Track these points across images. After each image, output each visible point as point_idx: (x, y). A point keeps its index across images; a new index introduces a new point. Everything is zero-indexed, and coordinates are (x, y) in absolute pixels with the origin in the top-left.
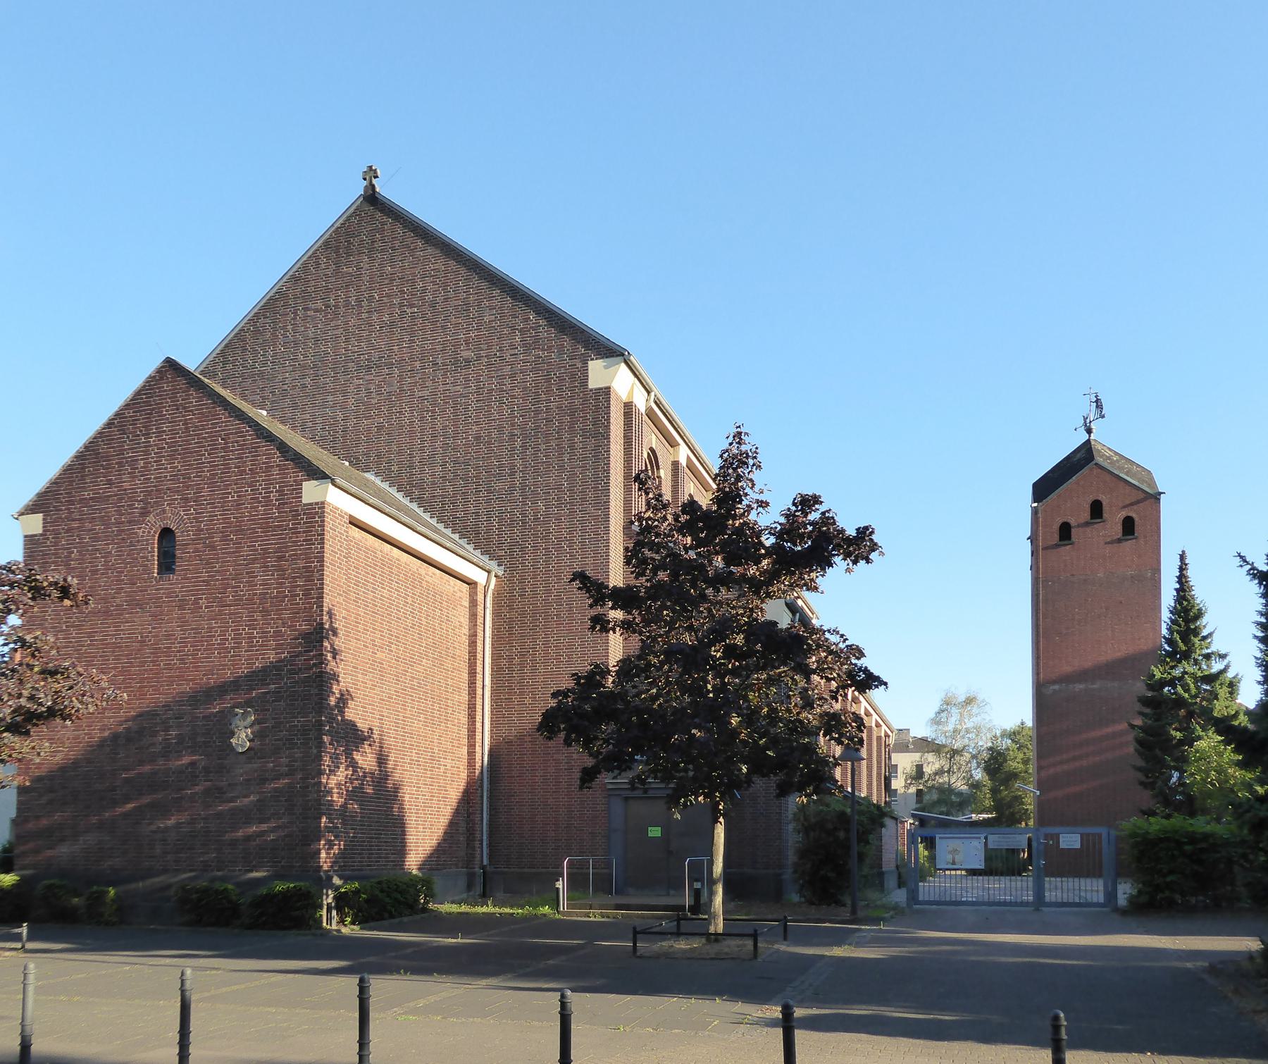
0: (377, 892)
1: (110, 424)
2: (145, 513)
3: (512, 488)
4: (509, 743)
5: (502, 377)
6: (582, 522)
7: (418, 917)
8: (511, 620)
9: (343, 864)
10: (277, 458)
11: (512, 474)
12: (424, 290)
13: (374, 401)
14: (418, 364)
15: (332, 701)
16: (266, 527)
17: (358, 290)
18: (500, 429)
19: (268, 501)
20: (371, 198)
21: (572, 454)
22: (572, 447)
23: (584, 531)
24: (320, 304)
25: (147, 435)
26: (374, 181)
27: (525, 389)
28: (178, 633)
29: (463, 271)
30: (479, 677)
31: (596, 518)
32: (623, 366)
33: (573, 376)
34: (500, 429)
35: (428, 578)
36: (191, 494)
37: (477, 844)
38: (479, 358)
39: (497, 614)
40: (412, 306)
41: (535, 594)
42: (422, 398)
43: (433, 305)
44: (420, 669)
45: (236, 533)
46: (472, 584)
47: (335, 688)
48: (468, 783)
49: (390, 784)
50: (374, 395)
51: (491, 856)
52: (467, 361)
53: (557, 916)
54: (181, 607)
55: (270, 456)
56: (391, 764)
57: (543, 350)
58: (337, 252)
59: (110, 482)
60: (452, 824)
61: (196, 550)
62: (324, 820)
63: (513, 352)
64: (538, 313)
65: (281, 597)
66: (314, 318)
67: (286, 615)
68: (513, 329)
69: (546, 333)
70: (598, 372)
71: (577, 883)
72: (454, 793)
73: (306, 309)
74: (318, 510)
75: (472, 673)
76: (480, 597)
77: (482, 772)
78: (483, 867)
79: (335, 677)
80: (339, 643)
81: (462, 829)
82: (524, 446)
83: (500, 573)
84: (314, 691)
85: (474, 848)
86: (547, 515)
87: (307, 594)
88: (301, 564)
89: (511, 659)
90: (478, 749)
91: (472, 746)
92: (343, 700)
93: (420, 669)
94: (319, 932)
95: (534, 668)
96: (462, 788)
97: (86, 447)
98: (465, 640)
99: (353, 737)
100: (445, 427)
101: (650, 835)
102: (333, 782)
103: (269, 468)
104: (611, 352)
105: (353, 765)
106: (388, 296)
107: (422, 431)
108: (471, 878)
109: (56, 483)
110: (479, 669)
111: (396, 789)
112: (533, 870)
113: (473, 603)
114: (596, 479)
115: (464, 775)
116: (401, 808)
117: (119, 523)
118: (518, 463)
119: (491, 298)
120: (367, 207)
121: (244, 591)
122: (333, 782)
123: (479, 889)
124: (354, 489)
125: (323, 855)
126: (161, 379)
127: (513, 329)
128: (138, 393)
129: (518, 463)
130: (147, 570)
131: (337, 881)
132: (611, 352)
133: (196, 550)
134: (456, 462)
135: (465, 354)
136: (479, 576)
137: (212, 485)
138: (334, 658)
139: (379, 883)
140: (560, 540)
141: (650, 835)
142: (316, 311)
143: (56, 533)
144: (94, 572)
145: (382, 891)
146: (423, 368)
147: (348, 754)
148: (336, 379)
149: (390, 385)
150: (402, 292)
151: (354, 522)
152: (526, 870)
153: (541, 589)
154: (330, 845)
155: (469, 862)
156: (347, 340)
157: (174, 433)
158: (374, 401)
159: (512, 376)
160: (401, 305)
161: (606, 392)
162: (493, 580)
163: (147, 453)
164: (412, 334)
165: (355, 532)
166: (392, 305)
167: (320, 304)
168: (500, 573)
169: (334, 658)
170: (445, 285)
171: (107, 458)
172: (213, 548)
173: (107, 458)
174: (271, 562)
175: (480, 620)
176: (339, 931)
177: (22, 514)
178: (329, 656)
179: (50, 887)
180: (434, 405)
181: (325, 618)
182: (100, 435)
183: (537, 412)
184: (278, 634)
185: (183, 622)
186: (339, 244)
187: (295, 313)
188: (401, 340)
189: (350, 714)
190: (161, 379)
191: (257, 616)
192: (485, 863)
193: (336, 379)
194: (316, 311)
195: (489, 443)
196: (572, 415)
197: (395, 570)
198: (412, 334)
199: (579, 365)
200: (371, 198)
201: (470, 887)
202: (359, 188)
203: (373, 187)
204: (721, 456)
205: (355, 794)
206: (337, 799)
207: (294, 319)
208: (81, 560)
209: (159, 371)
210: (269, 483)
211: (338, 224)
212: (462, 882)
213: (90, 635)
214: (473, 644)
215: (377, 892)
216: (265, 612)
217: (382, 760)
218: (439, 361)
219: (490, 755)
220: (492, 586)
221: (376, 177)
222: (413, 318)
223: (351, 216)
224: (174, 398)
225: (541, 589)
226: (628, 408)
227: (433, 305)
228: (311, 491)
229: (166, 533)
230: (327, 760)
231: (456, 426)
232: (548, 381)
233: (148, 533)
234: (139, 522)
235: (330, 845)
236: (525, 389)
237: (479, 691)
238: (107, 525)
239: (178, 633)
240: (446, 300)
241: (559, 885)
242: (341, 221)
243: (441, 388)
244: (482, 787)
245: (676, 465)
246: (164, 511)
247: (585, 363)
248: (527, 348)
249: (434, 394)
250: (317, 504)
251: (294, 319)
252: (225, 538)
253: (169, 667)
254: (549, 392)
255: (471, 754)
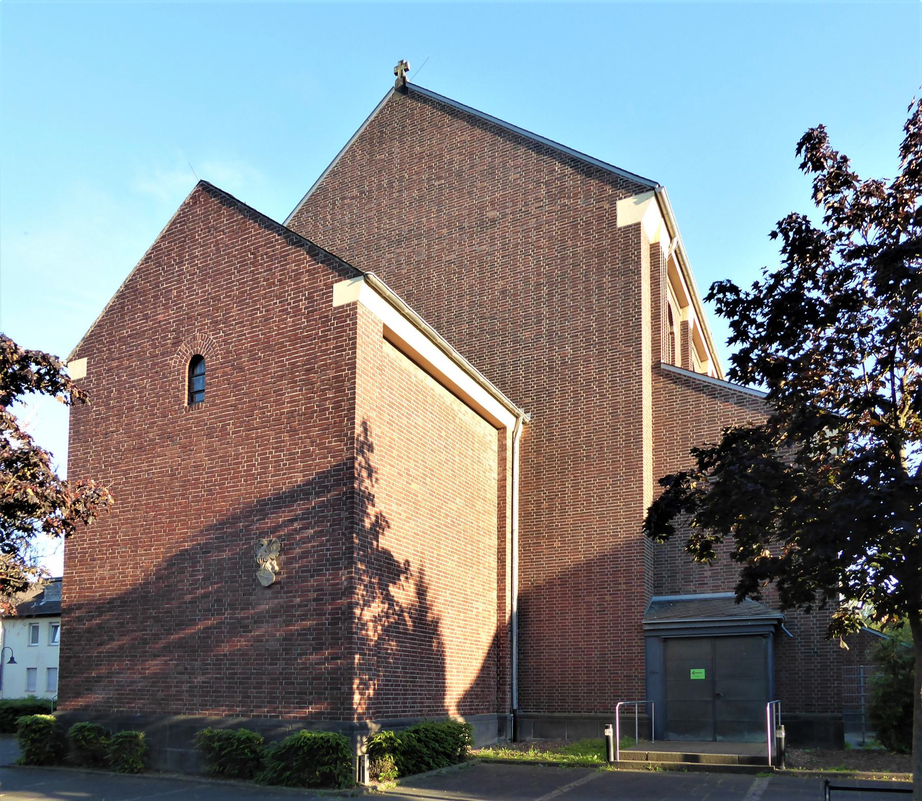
0: (415, 743)
1: (147, 259)
2: (177, 343)
3: (539, 335)
4: (538, 587)
5: (528, 231)
6: (612, 360)
7: (455, 767)
8: (539, 465)
9: (376, 707)
10: (307, 262)
11: (539, 322)
12: (451, 162)
13: (404, 272)
14: (445, 231)
15: (367, 524)
16: (294, 339)
17: (390, 174)
18: (526, 280)
19: (297, 310)
20: (403, 88)
21: (601, 295)
22: (600, 287)
23: (614, 369)
24: (355, 192)
25: (181, 263)
26: (405, 74)
27: (551, 238)
28: (207, 463)
29: (488, 136)
30: (508, 521)
31: (627, 355)
32: (653, 199)
33: (600, 218)
34: (526, 280)
35: (460, 415)
36: (220, 315)
37: (507, 688)
38: (504, 215)
39: (524, 460)
40: (439, 178)
41: (564, 438)
42: (450, 262)
43: (459, 174)
44: (454, 506)
45: (264, 350)
46: (501, 429)
47: (371, 510)
48: (498, 627)
49: (430, 616)
50: (404, 266)
51: (519, 700)
52: (493, 221)
53: (610, 769)
54: (210, 436)
55: (299, 262)
56: (430, 595)
57: (569, 198)
58: (371, 143)
59: (146, 317)
60: (484, 668)
61: (225, 374)
62: (357, 656)
63: (537, 205)
64: (563, 162)
65: (309, 413)
66: (350, 205)
67: (315, 432)
68: (538, 183)
69: (572, 179)
70: (628, 211)
71: (627, 729)
72: (486, 636)
73: (343, 199)
74: (350, 311)
75: (502, 517)
76: (509, 443)
77: (511, 617)
78: (513, 711)
79: (370, 498)
80: (374, 459)
81: (493, 674)
82: (550, 294)
83: (528, 420)
84: (344, 514)
85: (504, 692)
86: (575, 358)
87: (337, 407)
88: (331, 374)
89: (538, 503)
90: (508, 594)
91: (501, 590)
92: (381, 524)
93: (454, 506)
94: (349, 791)
95: (563, 511)
96: (493, 632)
97: (126, 286)
98: (494, 484)
99: (389, 569)
100: (471, 286)
101: (693, 677)
102: (367, 615)
103: (298, 275)
104: (639, 187)
105: (388, 598)
106: (417, 173)
107: (449, 292)
108: (502, 721)
109: (99, 325)
110: (508, 513)
111: (436, 623)
112: (566, 714)
113: (502, 448)
114: (626, 313)
115: (494, 619)
116: (441, 644)
117: (153, 356)
118: (545, 310)
119: (515, 158)
120: (400, 98)
121: (272, 412)
122: (367, 615)
123: (510, 734)
124: (389, 292)
125: (357, 697)
126: (195, 203)
127: (538, 183)
128: (173, 223)
129: (545, 310)
130: (178, 400)
131: (373, 726)
132: (639, 187)
133: (225, 374)
134: (482, 318)
135: (491, 214)
136: (507, 420)
137: (241, 302)
138: (370, 476)
139: (416, 732)
140: (588, 381)
141: (693, 677)
142: (352, 198)
143: (98, 374)
144: (130, 409)
145: (419, 740)
146: (450, 233)
147: (384, 588)
148: (369, 257)
149: (419, 254)
150: (431, 167)
151: (389, 337)
152: (557, 714)
153: (569, 432)
154: (365, 685)
155: (499, 708)
156: (379, 220)
157: (205, 255)
158: (404, 272)
159: (538, 228)
160: (429, 179)
161: (636, 228)
162: (521, 428)
163: (180, 281)
164: (440, 204)
165: (388, 347)
166: (421, 181)
167: (355, 192)
168: (528, 420)
169: (370, 476)
170: (471, 154)
171: (144, 293)
172: (241, 369)
173: (144, 293)
174: (300, 376)
175: (509, 465)
176: (375, 788)
177: (71, 360)
178: (364, 474)
179: (81, 730)
180: (461, 266)
181: (358, 430)
182: (139, 271)
183: (563, 259)
184: (306, 454)
185: (211, 451)
186: (374, 135)
187: (334, 204)
188: (430, 212)
189: (385, 542)
190: (195, 203)
191: (285, 437)
192: (515, 707)
193: (369, 257)
194: (352, 198)
195: (515, 295)
196: (600, 256)
197: (429, 400)
198: (440, 204)
199: (607, 206)
200: (403, 88)
201: (501, 731)
202: (391, 82)
203: (404, 78)
204: (907, 129)
205: (393, 630)
206: (372, 634)
207: (333, 209)
208: (119, 398)
209: (194, 197)
210: (298, 290)
211: (372, 118)
212: (494, 727)
213: (125, 473)
214: (502, 488)
215: (415, 743)
216: (293, 432)
217: (421, 591)
218: (466, 225)
219: (519, 600)
220: (519, 435)
221: (407, 70)
222: (441, 189)
223: (384, 108)
224: (206, 221)
225: (569, 432)
226: (655, 249)
227: (459, 174)
228: (345, 292)
229: (197, 360)
230: (360, 591)
231: (481, 283)
232: (575, 226)
233: (180, 362)
234: (172, 353)
235: (365, 685)
236: (551, 238)
237: (508, 536)
238: (142, 361)
239: (207, 463)
240: (472, 167)
241: (609, 732)
242: (375, 115)
243: (467, 250)
244: (511, 631)
245: (685, 324)
246: (195, 338)
247: (613, 204)
248: (552, 198)
249: (460, 256)
250: (348, 305)
251: (333, 209)
252: (253, 358)
253: (197, 499)
254: (575, 236)
255: (501, 598)
